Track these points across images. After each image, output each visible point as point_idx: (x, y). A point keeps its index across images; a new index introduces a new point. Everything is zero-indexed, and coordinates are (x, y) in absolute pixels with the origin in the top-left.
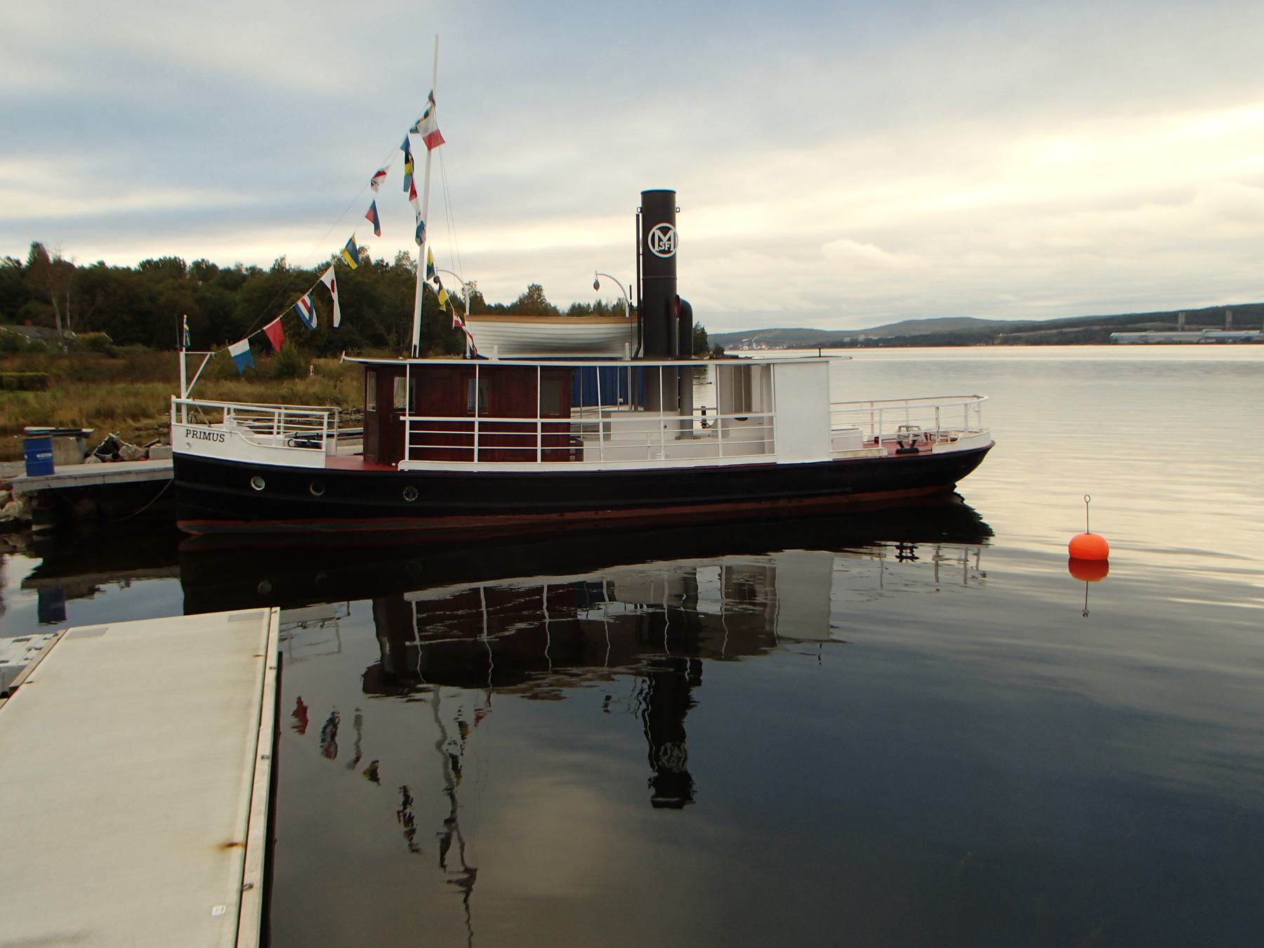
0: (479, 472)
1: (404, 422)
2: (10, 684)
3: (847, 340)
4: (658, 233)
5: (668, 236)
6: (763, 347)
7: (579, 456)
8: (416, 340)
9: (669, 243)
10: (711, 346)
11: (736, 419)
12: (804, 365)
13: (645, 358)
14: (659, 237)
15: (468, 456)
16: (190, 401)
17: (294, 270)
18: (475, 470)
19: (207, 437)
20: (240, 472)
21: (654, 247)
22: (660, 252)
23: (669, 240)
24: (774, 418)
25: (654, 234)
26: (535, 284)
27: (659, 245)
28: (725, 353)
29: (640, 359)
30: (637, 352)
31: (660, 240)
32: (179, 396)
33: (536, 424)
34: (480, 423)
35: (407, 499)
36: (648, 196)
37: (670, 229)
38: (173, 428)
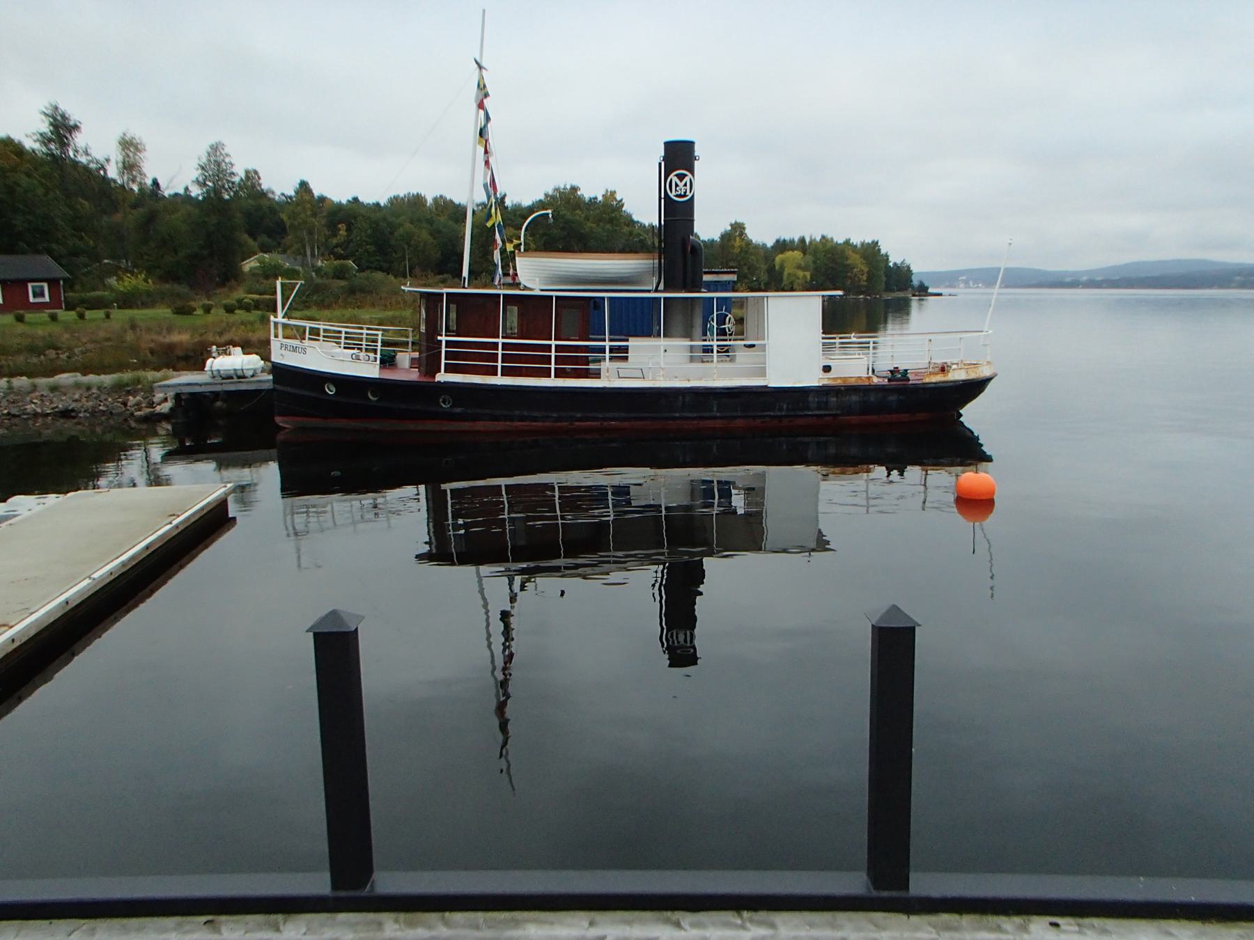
0: (501, 385)
1: (441, 341)
3: (1068, 280)
4: (675, 179)
6: (980, 285)
7: (597, 375)
8: (465, 273)
10: (915, 282)
11: (745, 345)
12: (792, 299)
13: (665, 291)
14: (676, 183)
15: (493, 371)
16: (285, 321)
17: (536, 202)
18: (499, 383)
19: (294, 349)
20: (316, 379)
21: (671, 191)
22: (677, 196)
23: (685, 185)
24: (767, 346)
25: (671, 180)
26: (738, 221)
27: (676, 190)
28: (930, 290)
29: (661, 291)
30: (657, 286)
31: (677, 185)
32: (276, 317)
33: (550, 345)
34: (503, 344)
35: (444, 406)
36: (669, 146)
37: (686, 175)
38: (272, 342)
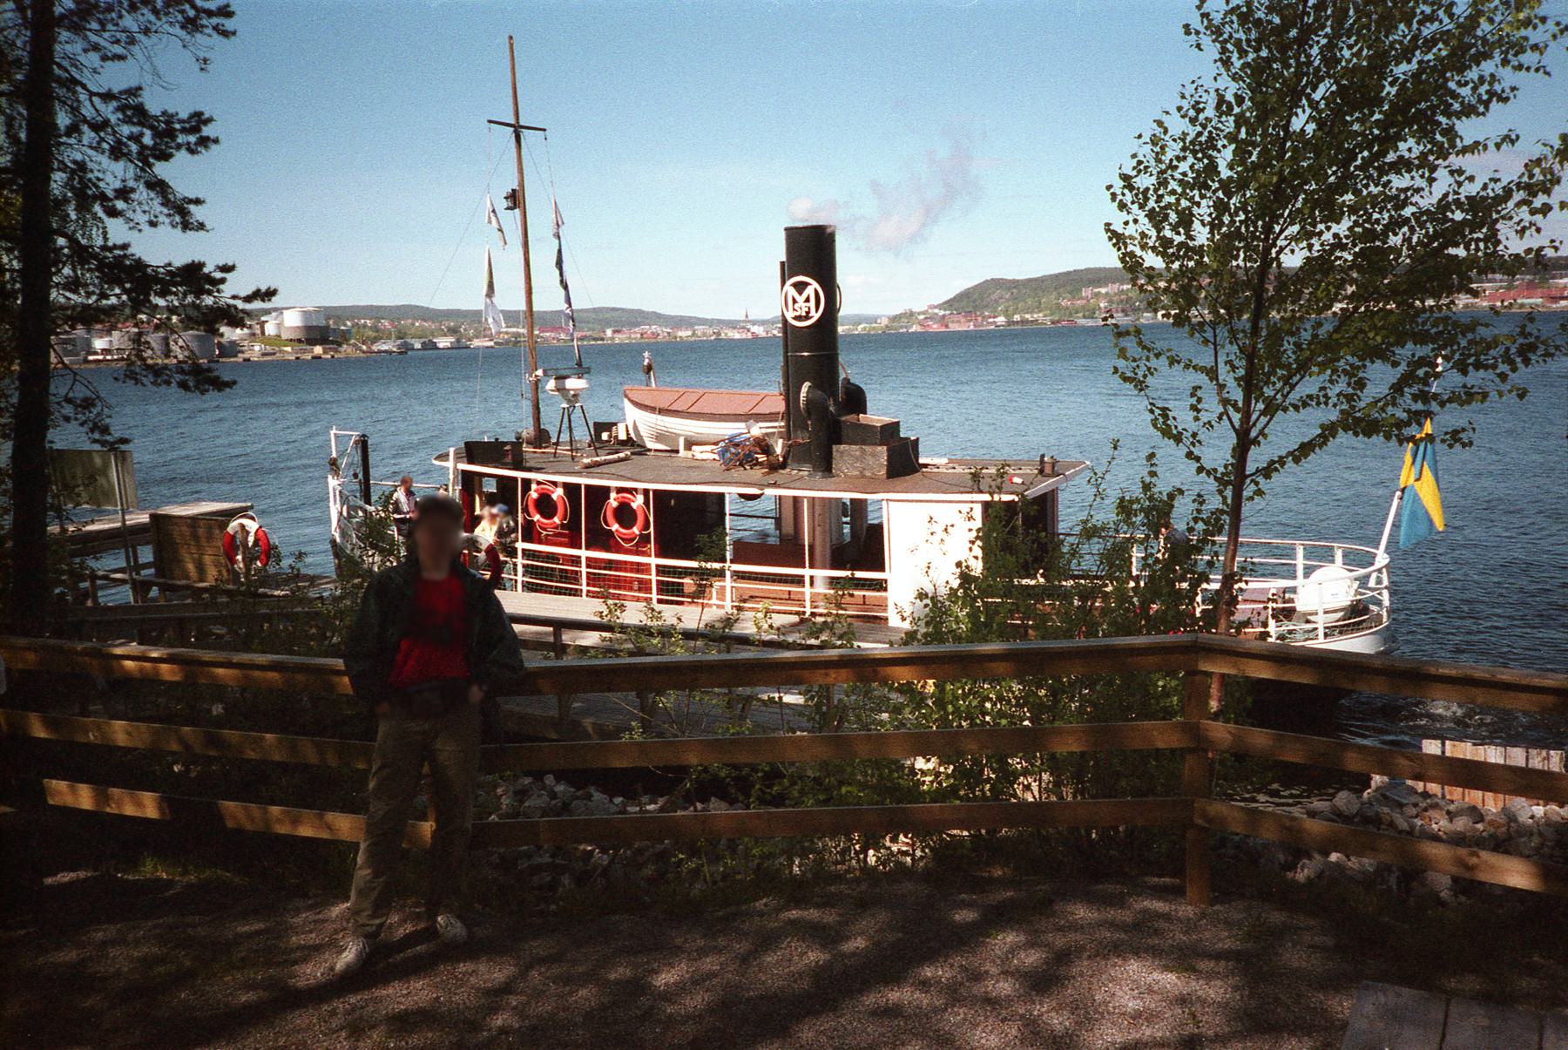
2: (174, 499)
4: (792, 292)
5: (805, 295)
9: (807, 304)
21: (816, 290)
22: (798, 318)
27: (794, 309)
31: (795, 301)
37: (806, 284)
